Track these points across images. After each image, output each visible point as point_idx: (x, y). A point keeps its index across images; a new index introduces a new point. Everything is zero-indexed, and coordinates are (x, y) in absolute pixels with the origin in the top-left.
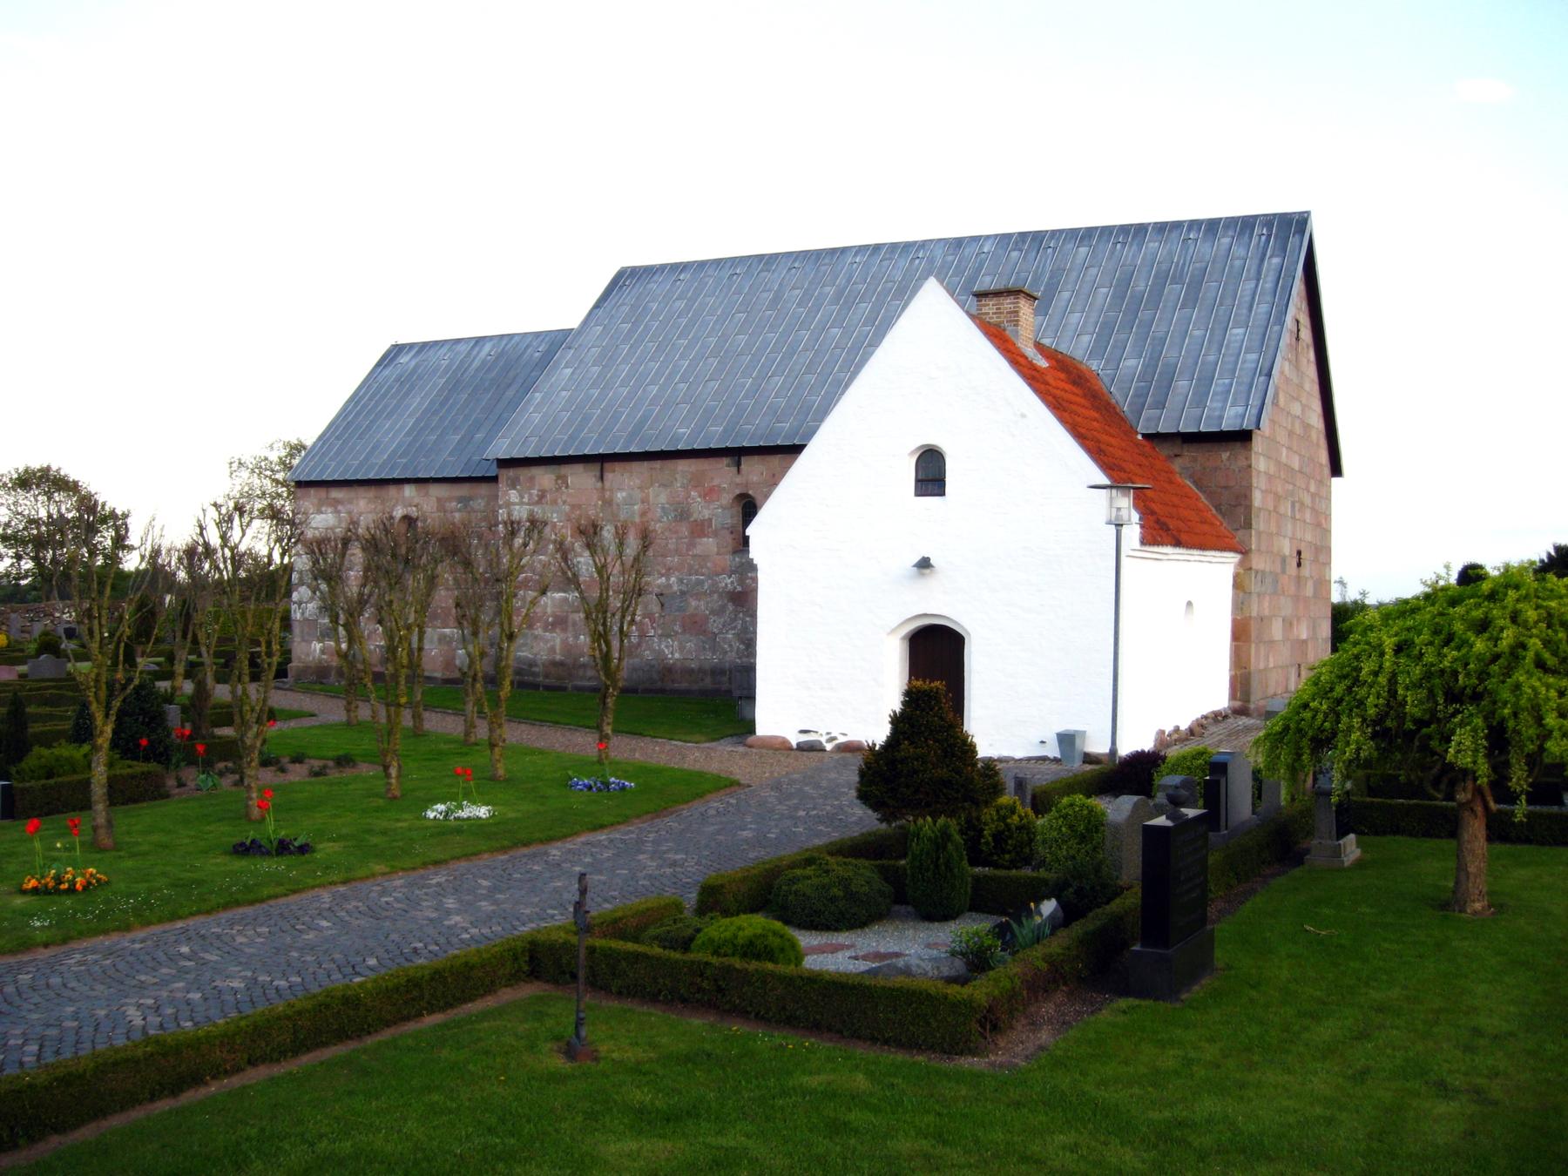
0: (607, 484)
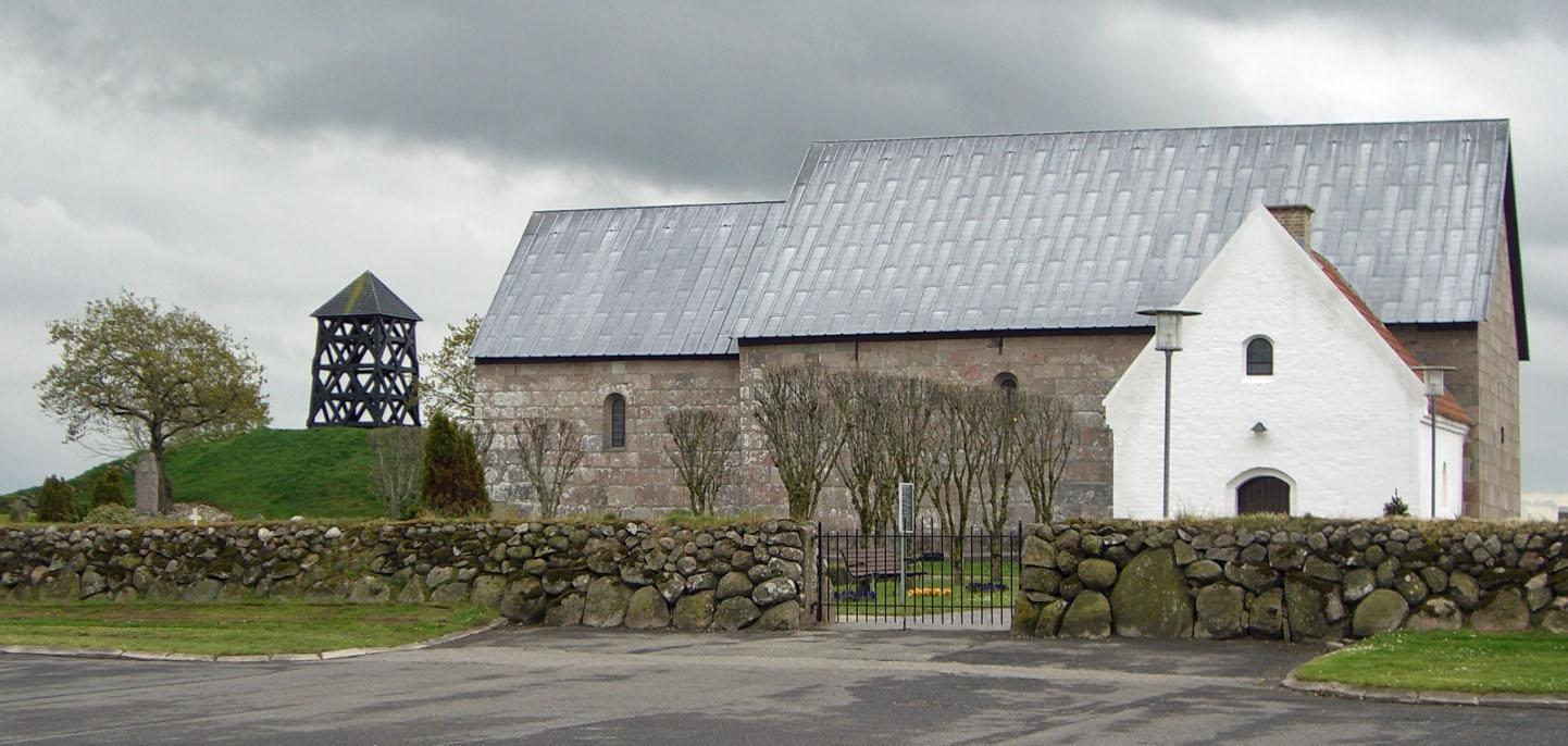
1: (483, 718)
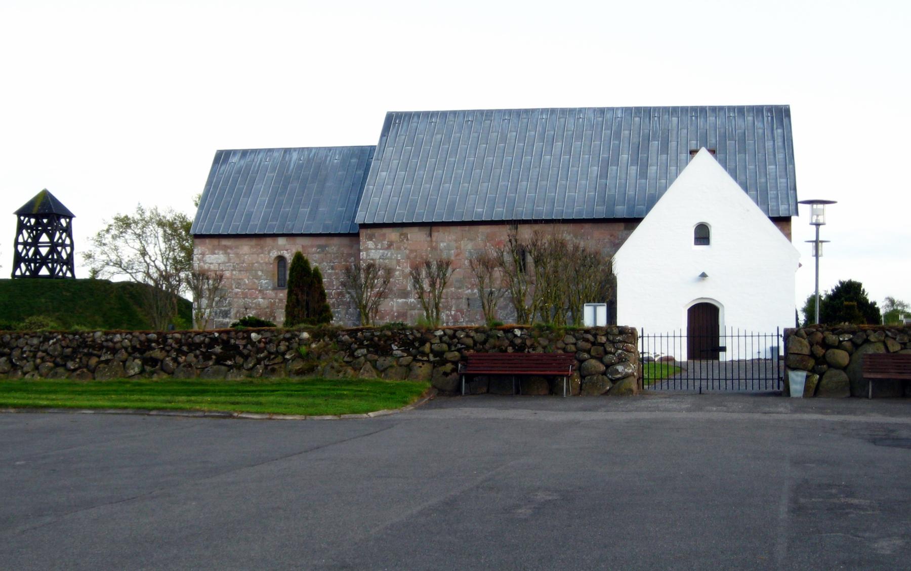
0: (434, 239)
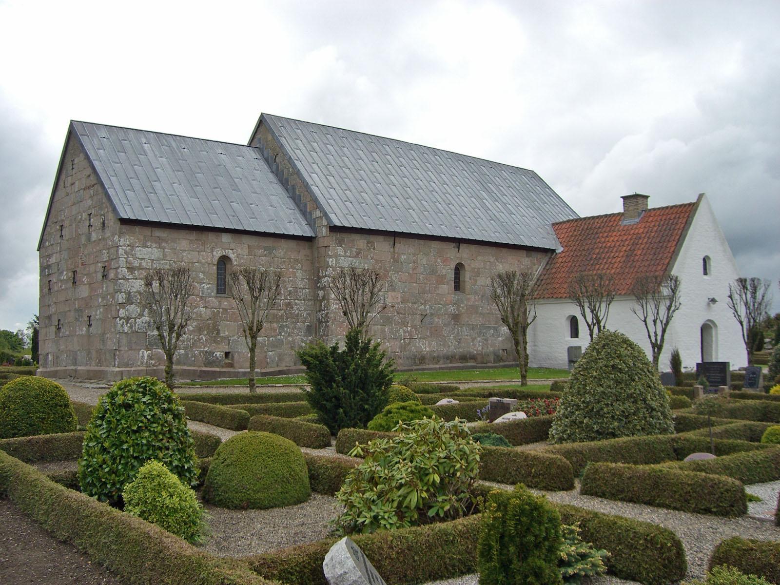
0: (396, 250)
1: (619, 522)
